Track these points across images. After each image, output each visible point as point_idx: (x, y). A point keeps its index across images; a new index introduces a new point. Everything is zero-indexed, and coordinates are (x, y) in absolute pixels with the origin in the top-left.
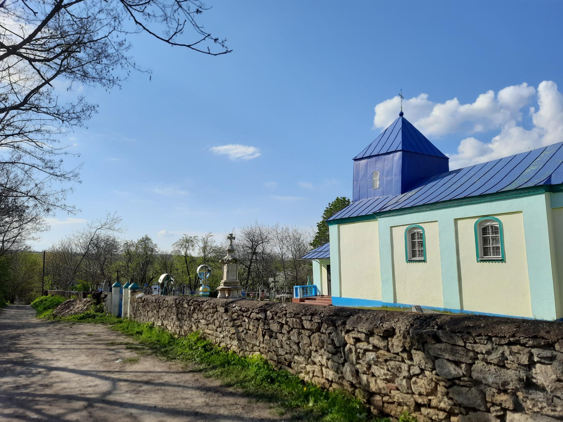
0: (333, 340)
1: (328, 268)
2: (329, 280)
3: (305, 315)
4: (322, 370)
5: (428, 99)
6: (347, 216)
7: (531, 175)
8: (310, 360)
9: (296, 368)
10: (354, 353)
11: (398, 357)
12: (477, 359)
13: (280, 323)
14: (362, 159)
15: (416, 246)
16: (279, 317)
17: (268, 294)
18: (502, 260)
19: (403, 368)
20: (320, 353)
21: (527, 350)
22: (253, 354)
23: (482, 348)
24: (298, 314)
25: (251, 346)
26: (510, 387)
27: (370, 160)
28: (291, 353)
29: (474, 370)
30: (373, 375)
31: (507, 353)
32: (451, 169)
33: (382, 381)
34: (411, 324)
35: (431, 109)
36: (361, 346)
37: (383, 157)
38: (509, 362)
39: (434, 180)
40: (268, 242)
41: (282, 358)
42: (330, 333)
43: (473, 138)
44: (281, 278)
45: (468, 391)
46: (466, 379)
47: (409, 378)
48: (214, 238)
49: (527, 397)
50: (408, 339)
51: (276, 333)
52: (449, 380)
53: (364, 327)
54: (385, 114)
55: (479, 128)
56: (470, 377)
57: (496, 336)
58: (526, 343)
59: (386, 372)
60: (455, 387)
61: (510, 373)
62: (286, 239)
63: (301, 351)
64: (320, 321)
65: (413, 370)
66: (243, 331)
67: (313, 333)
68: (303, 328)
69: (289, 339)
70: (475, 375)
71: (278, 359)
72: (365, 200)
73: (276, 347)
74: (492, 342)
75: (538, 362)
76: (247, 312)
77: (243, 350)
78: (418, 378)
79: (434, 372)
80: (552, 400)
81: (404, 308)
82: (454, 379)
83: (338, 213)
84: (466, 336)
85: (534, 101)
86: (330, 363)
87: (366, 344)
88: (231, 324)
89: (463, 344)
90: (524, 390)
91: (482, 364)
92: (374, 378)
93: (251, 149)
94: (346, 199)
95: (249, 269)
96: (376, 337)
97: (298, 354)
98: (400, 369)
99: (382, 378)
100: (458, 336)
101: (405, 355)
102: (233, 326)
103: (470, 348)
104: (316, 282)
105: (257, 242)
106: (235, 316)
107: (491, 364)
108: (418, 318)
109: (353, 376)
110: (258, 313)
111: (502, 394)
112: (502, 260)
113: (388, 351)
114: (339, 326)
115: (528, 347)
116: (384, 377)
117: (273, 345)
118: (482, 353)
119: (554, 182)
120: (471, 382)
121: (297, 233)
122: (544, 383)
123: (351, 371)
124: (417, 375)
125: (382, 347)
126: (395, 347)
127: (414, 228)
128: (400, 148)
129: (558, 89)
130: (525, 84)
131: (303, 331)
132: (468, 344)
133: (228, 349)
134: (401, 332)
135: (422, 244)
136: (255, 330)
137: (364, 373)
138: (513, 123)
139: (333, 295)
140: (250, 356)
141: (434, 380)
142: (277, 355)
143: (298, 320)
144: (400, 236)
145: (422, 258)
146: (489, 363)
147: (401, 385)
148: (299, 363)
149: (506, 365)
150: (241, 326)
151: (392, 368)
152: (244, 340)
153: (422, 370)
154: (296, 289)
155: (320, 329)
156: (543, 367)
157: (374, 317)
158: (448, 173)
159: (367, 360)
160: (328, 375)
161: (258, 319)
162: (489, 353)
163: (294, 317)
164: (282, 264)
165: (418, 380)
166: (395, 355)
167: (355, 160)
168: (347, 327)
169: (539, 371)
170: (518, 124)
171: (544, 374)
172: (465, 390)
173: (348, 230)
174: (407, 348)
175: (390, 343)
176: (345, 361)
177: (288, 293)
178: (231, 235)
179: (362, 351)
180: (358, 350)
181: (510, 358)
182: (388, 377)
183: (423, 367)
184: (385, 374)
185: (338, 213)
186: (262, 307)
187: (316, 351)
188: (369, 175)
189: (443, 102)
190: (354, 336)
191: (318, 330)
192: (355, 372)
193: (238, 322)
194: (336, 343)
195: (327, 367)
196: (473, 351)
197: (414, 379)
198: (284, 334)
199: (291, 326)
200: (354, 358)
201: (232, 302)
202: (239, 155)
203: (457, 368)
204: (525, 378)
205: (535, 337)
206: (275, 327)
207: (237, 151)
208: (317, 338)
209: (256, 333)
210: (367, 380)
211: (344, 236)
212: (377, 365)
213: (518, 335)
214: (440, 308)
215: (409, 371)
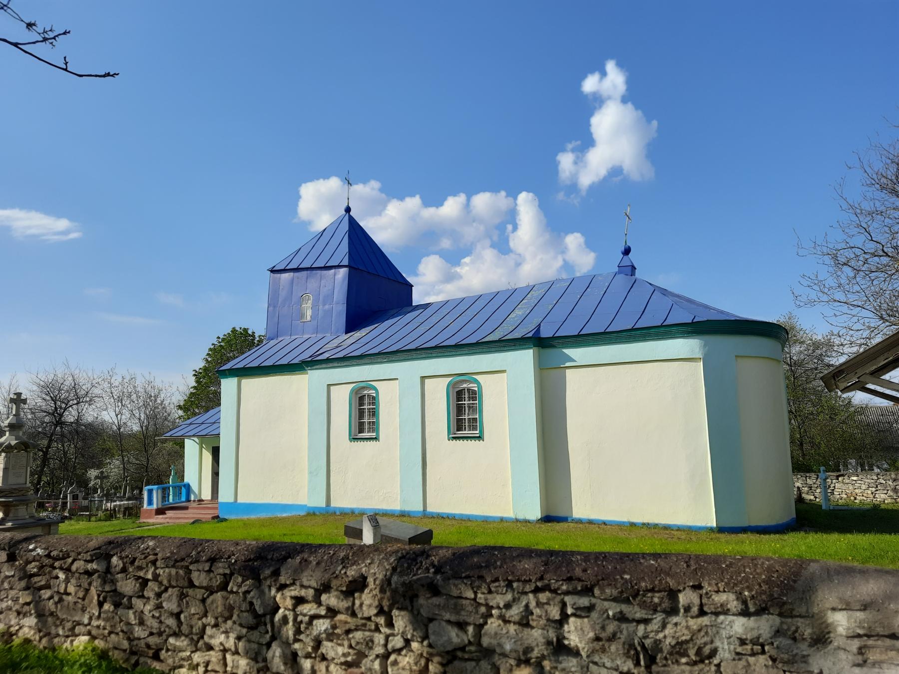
0: (251, 604)
1: (216, 452)
2: (216, 474)
3: (197, 561)
4: (224, 658)
5: (381, 190)
6: (255, 364)
7: (519, 322)
8: (201, 643)
9: (170, 661)
10: (291, 624)
11: (369, 623)
12: (491, 615)
13: (140, 577)
15: (365, 417)
16: (140, 568)
17: (85, 503)
18: (479, 437)
19: (376, 641)
20: (221, 630)
21: (559, 598)
22: (72, 641)
23: (499, 600)
24: (183, 560)
25: (69, 625)
26: (535, 653)
27: (297, 274)
28: (160, 634)
29: (486, 634)
30: (324, 658)
31: (533, 604)
32: (415, 303)
33: (338, 667)
34: (393, 568)
35: (384, 205)
36: (305, 611)
37: (319, 272)
38: (534, 617)
39: (393, 316)
40: (90, 402)
41: (142, 643)
42: (247, 592)
43: (437, 257)
44: (114, 467)
45: (475, 667)
46: (473, 648)
47: (385, 657)
49: (556, 668)
50: (388, 594)
51: (130, 597)
52: (448, 652)
53: (311, 578)
54: (318, 203)
55: (446, 243)
56: (479, 644)
57: (518, 580)
58: (558, 589)
59: (346, 650)
60: (456, 663)
61: (536, 634)
62: (130, 396)
63: (185, 629)
64: (228, 571)
65: (393, 643)
66: (51, 597)
67: (212, 593)
68: (191, 585)
69: (159, 607)
70: (485, 641)
71: (131, 646)
72: (287, 339)
73: (128, 624)
74: (513, 590)
75: (574, 615)
76: (64, 558)
77: (48, 634)
78: (399, 654)
79: (425, 643)
80: (588, 668)
81: (341, 514)
82: (455, 650)
83: (234, 356)
84: (477, 584)
85: (511, 217)
86: (241, 645)
87: (315, 606)
88: (23, 584)
89: (473, 596)
90: (552, 658)
91: (497, 624)
92: (325, 663)
93: (63, 224)
94: (250, 332)
95: (45, 454)
96: (334, 593)
97: (176, 635)
98: (370, 644)
99: (339, 661)
100: (466, 584)
101: (381, 620)
102: (27, 588)
103: (482, 601)
104: (190, 477)
105: (66, 402)
106: (32, 568)
107: (509, 622)
108: (403, 557)
109: (285, 664)
110: (91, 561)
111: (523, 666)
113: (354, 614)
114: (265, 579)
115: (560, 594)
116: (343, 660)
117: (121, 621)
118: (498, 607)
119: (545, 333)
120: (480, 651)
121: (153, 387)
122: (579, 645)
123: (284, 656)
124: (398, 651)
125: (343, 611)
126: (364, 608)
127: (364, 388)
128: (346, 262)
129: (539, 206)
130: (503, 193)
131: (191, 592)
132: (479, 595)
133: (11, 635)
134: (377, 582)
135: (374, 413)
136: (81, 594)
137: (308, 656)
138: (488, 242)
139: (221, 499)
140: (67, 645)
141: (425, 655)
142: (129, 639)
143: (181, 572)
144: (342, 399)
145: (374, 435)
146: (506, 622)
147: (370, 669)
148: (176, 650)
149: (531, 622)
150: (47, 587)
151: (358, 643)
152: (52, 614)
153: (407, 642)
154: (150, 492)
155: (227, 585)
156: (579, 621)
157: (331, 557)
158: (411, 308)
159: (315, 633)
160: (237, 667)
161: (89, 573)
162: (508, 606)
163: (173, 566)
164: (118, 440)
165: (400, 658)
166: (364, 621)
167: (273, 271)
168: (283, 579)
169: (572, 628)
170: (493, 246)
171: (580, 632)
172: (470, 665)
173: (255, 388)
174: (386, 608)
175: (357, 602)
176: (273, 638)
177: (129, 499)
179: (307, 618)
180: (299, 618)
181: (537, 611)
182: (349, 659)
183: (409, 637)
184: (344, 655)
185: (234, 356)
186: (99, 548)
187: (216, 625)
188: (294, 299)
189: (402, 199)
190: (293, 593)
191: (224, 587)
192: (289, 656)
193: (40, 581)
194: (257, 608)
195: (236, 652)
196: (487, 605)
197: (393, 657)
198: (148, 598)
199: (165, 582)
200: (291, 633)
201: (28, 540)
202: (33, 231)
203: (461, 634)
204: (555, 639)
205: (569, 579)
206: (127, 586)
207: (30, 222)
208: (220, 602)
209: (83, 599)
210: (313, 667)
211: (248, 401)
212: (332, 641)
213: (547, 576)
214: (395, 511)
215: (386, 645)
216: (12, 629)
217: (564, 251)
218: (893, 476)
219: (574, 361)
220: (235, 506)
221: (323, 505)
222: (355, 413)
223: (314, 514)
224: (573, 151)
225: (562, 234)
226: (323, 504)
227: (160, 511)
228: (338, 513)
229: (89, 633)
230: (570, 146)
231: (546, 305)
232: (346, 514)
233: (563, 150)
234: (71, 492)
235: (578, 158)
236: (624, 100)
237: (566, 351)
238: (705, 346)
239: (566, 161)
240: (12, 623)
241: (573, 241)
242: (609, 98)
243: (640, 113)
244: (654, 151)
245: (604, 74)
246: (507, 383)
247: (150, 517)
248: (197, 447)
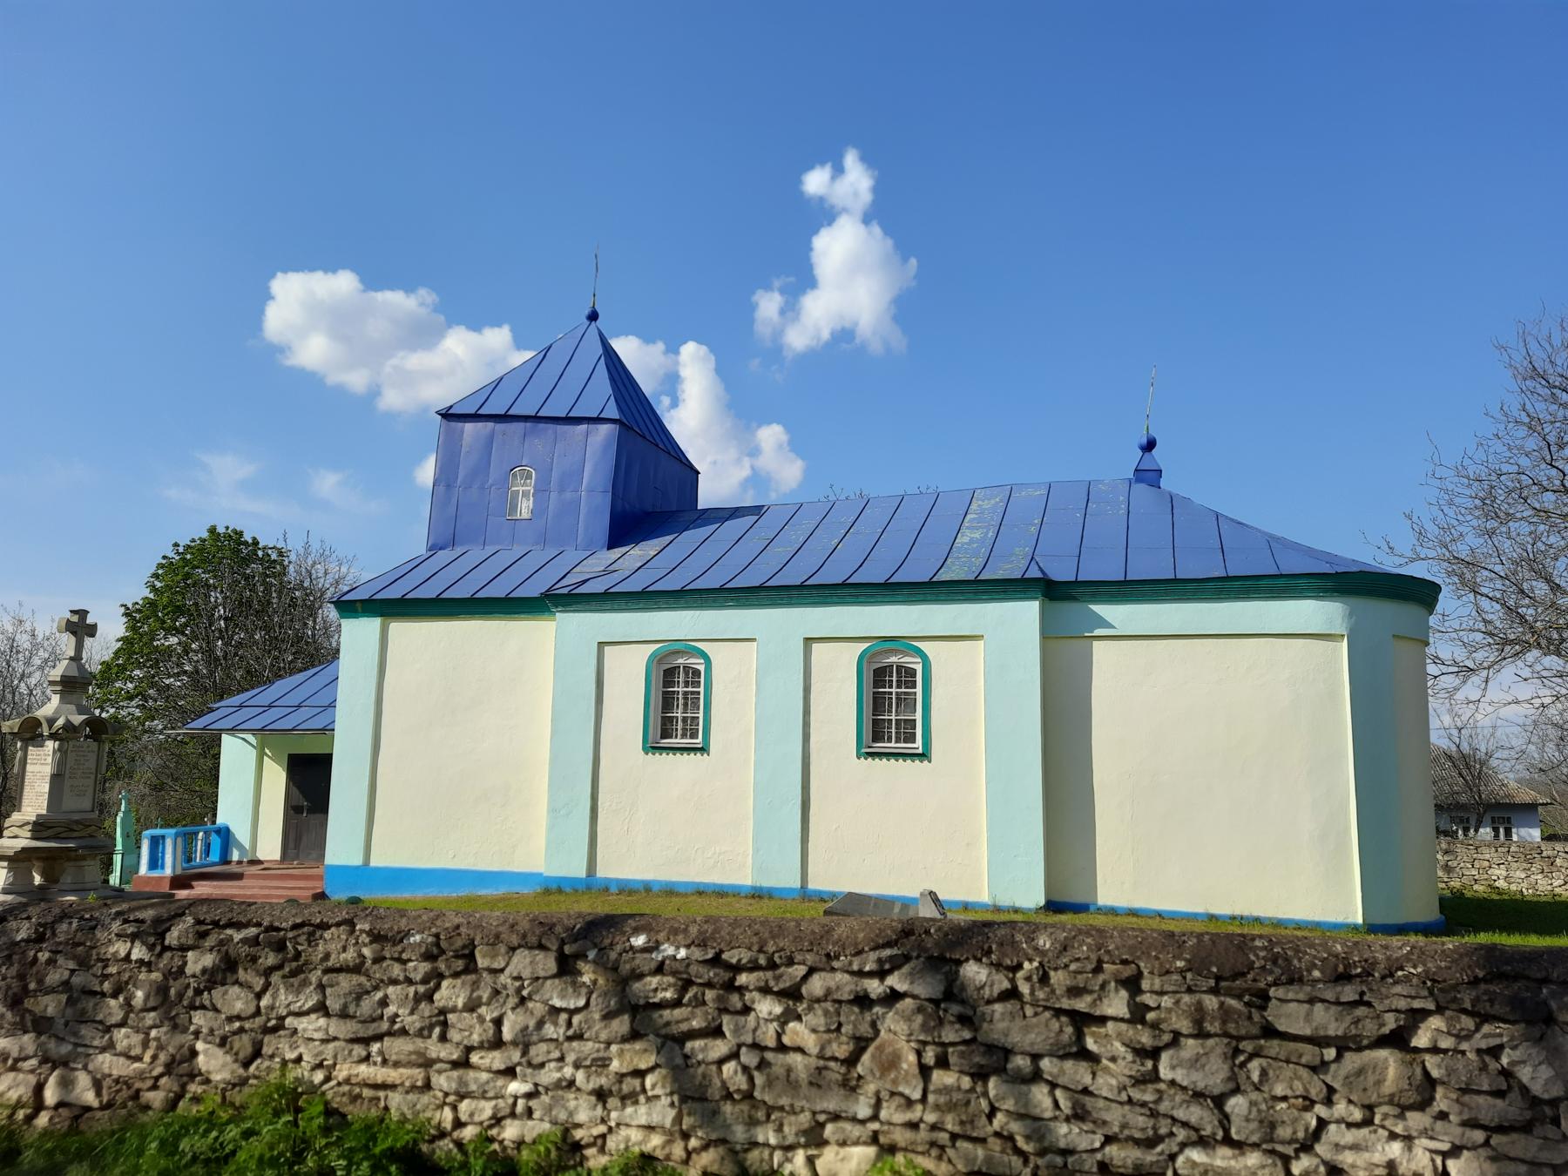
5: (436, 309)
14: (475, 417)
15: (677, 708)
18: (923, 755)
27: (500, 427)
37: (551, 426)
72: (476, 554)
88: (621, 1025)
112: (924, 756)
127: (677, 653)
135: (691, 701)
154: (156, 842)
178: (83, 614)
189: (476, 326)
206: (1024, 1031)
216: (578, 1134)
217: (754, 452)
218: (1444, 846)
219: (1111, 626)
220: (365, 871)
221: (582, 874)
222: (656, 700)
223: (560, 891)
224: (782, 291)
225: (754, 425)
228: (614, 890)
229: (874, 1139)
230: (777, 283)
231: (795, 535)
232: (631, 892)
233: (768, 288)
235: (787, 302)
236: (867, 220)
237: (1092, 607)
238: (1351, 615)
239: (769, 305)
240: (582, 1117)
241: (771, 436)
242: (845, 210)
243: (890, 242)
244: (905, 309)
245: (839, 170)
246: (982, 661)
248: (253, 753)
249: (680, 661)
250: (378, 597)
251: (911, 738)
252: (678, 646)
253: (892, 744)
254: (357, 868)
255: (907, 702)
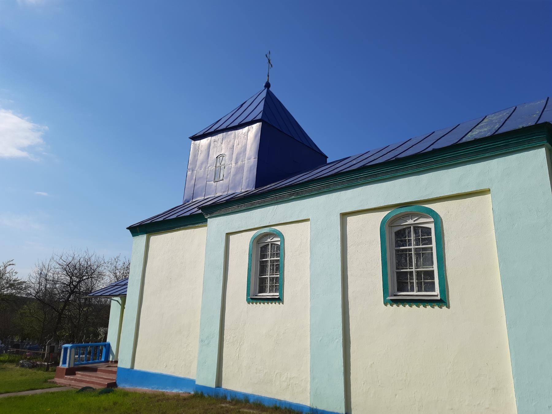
15: (266, 277)
48: (15, 268)
81: (233, 400)
95: (60, 314)
112: (443, 302)
127: (267, 235)
135: (278, 267)
221: (213, 385)
222: (256, 268)
226: (212, 384)
227: (71, 372)
234: (50, 344)
247: (61, 377)
249: (269, 240)
250: (500, 131)
251: (431, 287)
252: (266, 230)
253: (414, 293)
254: (128, 370)
255: (424, 256)
